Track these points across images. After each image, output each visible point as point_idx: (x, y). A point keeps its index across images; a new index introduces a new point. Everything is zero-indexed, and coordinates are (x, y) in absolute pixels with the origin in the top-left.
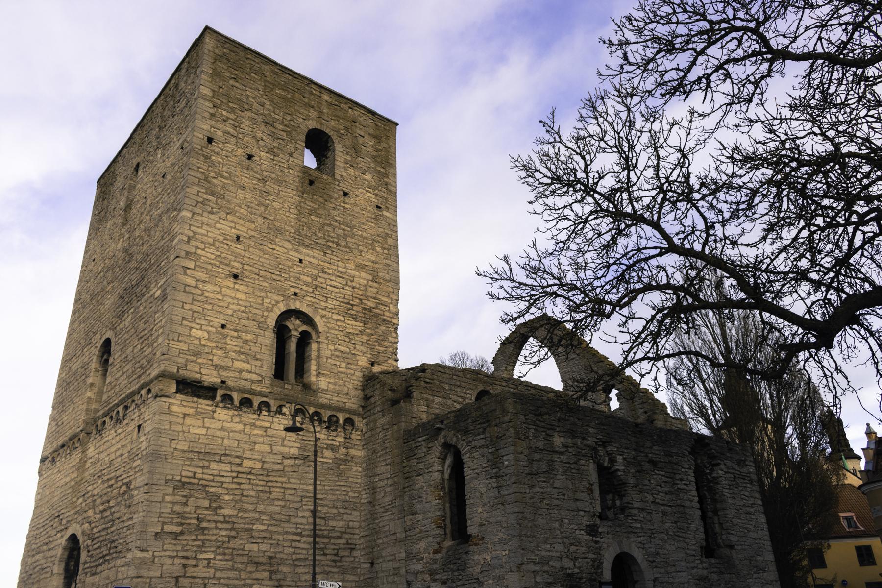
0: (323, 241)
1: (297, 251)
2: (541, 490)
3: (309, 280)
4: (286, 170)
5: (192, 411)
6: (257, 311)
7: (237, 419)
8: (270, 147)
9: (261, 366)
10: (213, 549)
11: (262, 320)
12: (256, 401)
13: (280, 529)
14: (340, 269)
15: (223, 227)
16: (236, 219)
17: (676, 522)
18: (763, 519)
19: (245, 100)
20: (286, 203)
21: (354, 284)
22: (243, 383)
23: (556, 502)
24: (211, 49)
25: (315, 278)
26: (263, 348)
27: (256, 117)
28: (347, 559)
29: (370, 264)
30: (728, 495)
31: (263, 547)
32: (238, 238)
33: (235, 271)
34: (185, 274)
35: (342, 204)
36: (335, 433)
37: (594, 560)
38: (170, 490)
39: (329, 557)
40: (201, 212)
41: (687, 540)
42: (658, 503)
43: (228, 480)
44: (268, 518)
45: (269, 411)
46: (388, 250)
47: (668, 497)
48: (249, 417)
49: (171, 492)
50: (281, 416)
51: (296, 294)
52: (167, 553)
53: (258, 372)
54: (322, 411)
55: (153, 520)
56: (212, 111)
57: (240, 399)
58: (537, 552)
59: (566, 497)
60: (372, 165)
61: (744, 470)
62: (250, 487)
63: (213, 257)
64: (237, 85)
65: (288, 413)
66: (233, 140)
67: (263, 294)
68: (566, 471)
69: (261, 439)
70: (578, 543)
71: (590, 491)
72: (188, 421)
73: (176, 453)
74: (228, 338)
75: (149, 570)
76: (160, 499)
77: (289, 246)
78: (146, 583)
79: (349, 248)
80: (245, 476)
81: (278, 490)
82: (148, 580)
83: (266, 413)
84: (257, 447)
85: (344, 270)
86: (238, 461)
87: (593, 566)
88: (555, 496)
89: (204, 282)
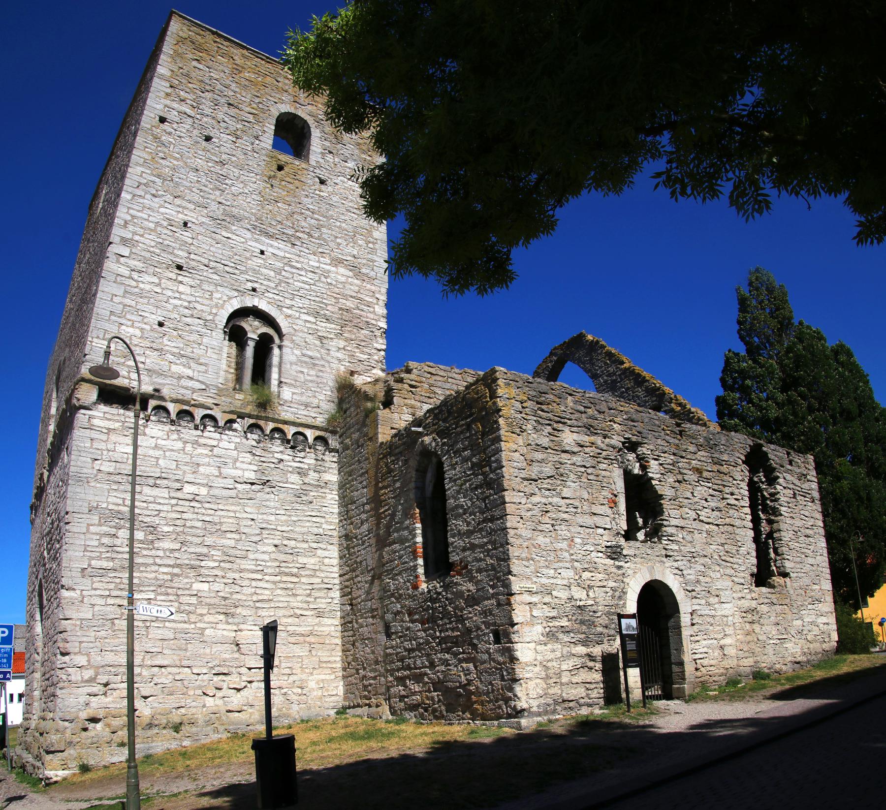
0: (290, 232)
1: (257, 241)
2: (544, 500)
3: (272, 274)
4: (250, 153)
5: (117, 425)
6: (204, 308)
7: (175, 436)
8: (232, 129)
9: (206, 372)
10: (152, 588)
11: (210, 317)
12: (199, 413)
13: (235, 566)
14: (311, 263)
15: (167, 211)
16: (185, 204)
17: (723, 545)
18: (823, 543)
19: (207, 81)
20: (248, 187)
21: (329, 280)
22: (183, 391)
23: (565, 516)
24: (175, 31)
25: (278, 272)
26: (210, 350)
27: (219, 98)
28: (324, 601)
29: (349, 258)
30: (786, 514)
31: (216, 587)
32: (185, 224)
33: (180, 261)
34: (118, 262)
35: (317, 192)
36: (302, 454)
37: (614, 590)
38: (95, 519)
39: (299, 598)
40: (143, 194)
41: (735, 566)
42: (702, 521)
43: (165, 508)
44: (219, 553)
45: (216, 426)
46: (373, 243)
47: (716, 513)
48: (189, 433)
49: (97, 522)
50: (231, 433)
51: (254, 290)
52: (98, 592)
53: (200, 379)
54: (285, 427)
55: (77, 554)
56: (169, 90)
57: (177, 410)
58: (535, 579)
59: (579, 510)
60: (357, 152)
61: (806, 486)
62: (195, 516)
63: (153, 244)
64: (201, 66)
65: (239, 429)
66: (190, 121)
67: (211, 288)
68: (580, 477)
69: (207, 460)
70: (592, 568)
71: (614, 504)
72: (113, 437)
73: (100, 476)
74: (166, 338)
75: (78, 611)
76: (84, 530)
77: (249, 235)
78: (76, 625)
79: (324, 240)
80: (187, 503)
81: (231, 521)
82: (78, 623)
83: (213, 429)
84: (201, 469)
85: (317, 264)
86: (178, 485)
87: (613, 597)
88: (564, 509)
89: (140, 272)
